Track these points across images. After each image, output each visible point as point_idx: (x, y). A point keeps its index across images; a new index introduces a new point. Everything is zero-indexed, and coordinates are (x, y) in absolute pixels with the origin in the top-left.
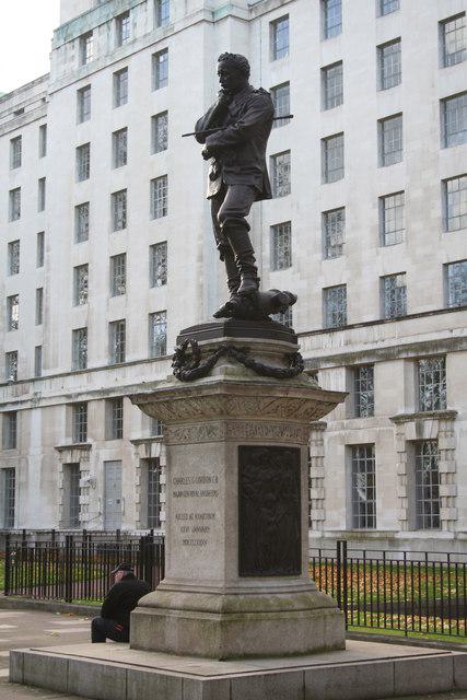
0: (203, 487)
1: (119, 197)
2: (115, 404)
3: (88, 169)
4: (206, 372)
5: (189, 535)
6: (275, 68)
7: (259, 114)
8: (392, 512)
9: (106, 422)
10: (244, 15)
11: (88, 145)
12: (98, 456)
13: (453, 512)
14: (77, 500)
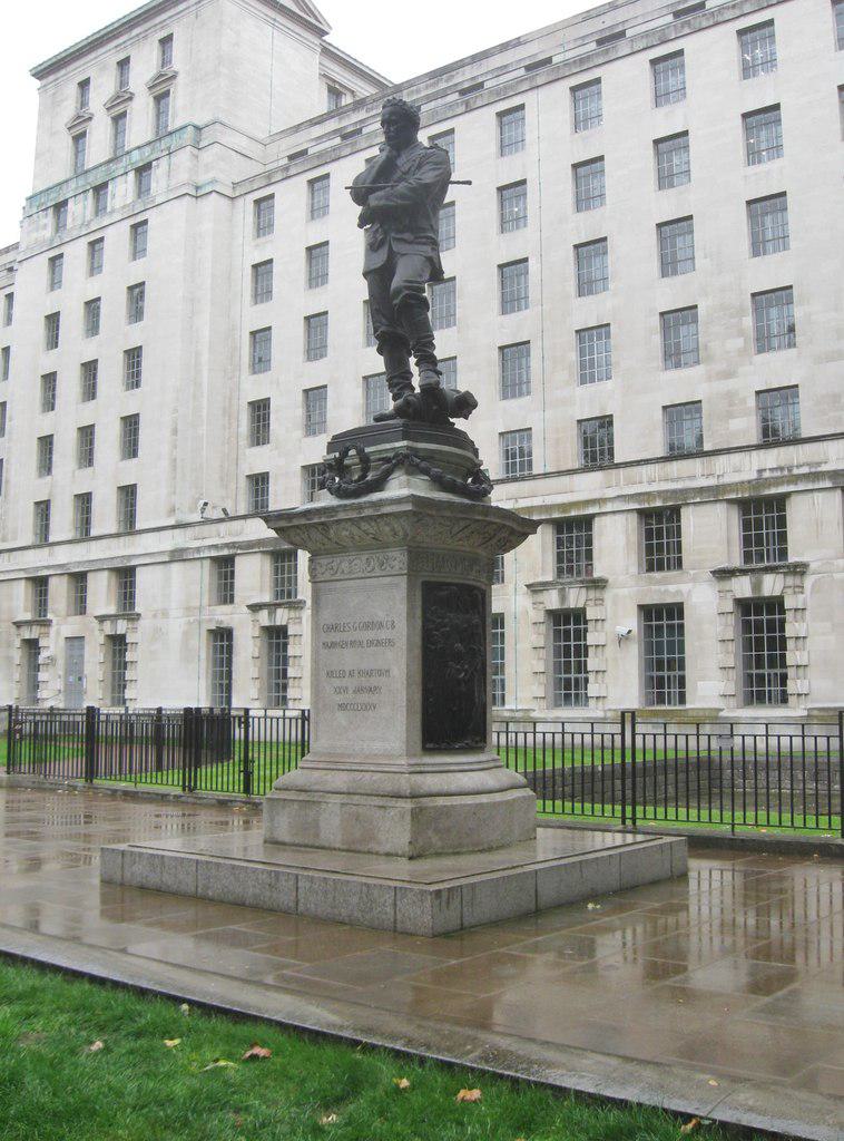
0: (370, 635)
1: (90, 369)
2: (79, 579)
3: (57, 338)
4: (379, 485)
5: (349, 697)
6: (257, 245)
7: (437, 173)
8: (711, 677)
9: (68, 597)
10: (228, 192)
11: (58, 314)
12: (58, 633)
13: (816, 683)
14: (36, 676)
